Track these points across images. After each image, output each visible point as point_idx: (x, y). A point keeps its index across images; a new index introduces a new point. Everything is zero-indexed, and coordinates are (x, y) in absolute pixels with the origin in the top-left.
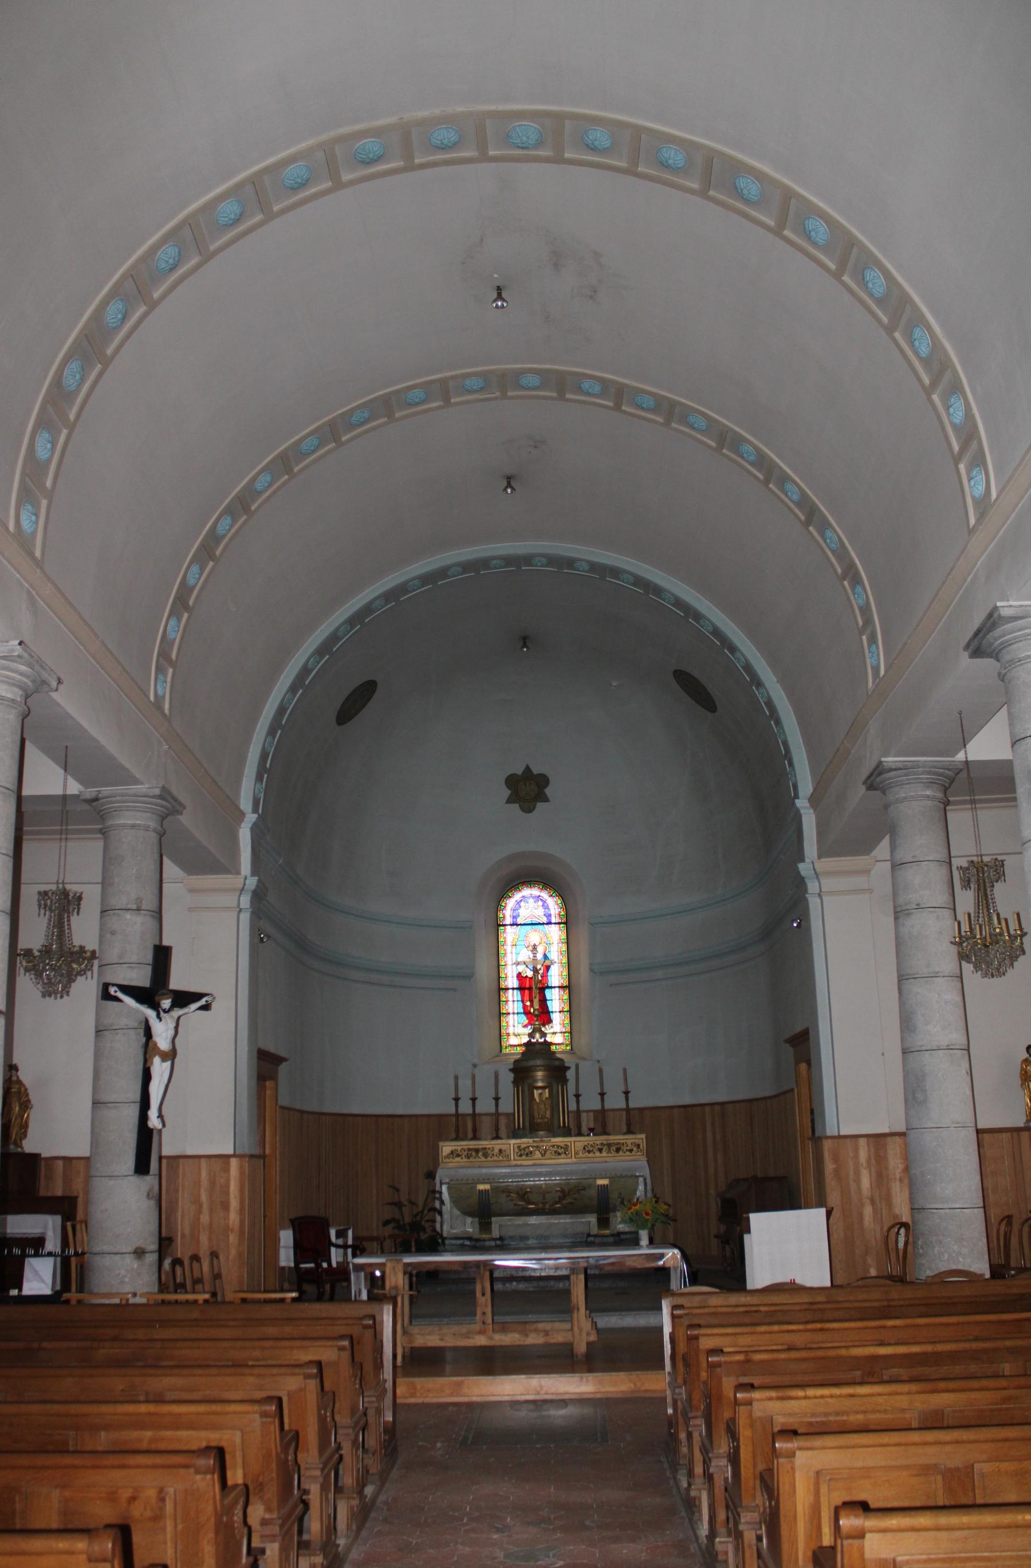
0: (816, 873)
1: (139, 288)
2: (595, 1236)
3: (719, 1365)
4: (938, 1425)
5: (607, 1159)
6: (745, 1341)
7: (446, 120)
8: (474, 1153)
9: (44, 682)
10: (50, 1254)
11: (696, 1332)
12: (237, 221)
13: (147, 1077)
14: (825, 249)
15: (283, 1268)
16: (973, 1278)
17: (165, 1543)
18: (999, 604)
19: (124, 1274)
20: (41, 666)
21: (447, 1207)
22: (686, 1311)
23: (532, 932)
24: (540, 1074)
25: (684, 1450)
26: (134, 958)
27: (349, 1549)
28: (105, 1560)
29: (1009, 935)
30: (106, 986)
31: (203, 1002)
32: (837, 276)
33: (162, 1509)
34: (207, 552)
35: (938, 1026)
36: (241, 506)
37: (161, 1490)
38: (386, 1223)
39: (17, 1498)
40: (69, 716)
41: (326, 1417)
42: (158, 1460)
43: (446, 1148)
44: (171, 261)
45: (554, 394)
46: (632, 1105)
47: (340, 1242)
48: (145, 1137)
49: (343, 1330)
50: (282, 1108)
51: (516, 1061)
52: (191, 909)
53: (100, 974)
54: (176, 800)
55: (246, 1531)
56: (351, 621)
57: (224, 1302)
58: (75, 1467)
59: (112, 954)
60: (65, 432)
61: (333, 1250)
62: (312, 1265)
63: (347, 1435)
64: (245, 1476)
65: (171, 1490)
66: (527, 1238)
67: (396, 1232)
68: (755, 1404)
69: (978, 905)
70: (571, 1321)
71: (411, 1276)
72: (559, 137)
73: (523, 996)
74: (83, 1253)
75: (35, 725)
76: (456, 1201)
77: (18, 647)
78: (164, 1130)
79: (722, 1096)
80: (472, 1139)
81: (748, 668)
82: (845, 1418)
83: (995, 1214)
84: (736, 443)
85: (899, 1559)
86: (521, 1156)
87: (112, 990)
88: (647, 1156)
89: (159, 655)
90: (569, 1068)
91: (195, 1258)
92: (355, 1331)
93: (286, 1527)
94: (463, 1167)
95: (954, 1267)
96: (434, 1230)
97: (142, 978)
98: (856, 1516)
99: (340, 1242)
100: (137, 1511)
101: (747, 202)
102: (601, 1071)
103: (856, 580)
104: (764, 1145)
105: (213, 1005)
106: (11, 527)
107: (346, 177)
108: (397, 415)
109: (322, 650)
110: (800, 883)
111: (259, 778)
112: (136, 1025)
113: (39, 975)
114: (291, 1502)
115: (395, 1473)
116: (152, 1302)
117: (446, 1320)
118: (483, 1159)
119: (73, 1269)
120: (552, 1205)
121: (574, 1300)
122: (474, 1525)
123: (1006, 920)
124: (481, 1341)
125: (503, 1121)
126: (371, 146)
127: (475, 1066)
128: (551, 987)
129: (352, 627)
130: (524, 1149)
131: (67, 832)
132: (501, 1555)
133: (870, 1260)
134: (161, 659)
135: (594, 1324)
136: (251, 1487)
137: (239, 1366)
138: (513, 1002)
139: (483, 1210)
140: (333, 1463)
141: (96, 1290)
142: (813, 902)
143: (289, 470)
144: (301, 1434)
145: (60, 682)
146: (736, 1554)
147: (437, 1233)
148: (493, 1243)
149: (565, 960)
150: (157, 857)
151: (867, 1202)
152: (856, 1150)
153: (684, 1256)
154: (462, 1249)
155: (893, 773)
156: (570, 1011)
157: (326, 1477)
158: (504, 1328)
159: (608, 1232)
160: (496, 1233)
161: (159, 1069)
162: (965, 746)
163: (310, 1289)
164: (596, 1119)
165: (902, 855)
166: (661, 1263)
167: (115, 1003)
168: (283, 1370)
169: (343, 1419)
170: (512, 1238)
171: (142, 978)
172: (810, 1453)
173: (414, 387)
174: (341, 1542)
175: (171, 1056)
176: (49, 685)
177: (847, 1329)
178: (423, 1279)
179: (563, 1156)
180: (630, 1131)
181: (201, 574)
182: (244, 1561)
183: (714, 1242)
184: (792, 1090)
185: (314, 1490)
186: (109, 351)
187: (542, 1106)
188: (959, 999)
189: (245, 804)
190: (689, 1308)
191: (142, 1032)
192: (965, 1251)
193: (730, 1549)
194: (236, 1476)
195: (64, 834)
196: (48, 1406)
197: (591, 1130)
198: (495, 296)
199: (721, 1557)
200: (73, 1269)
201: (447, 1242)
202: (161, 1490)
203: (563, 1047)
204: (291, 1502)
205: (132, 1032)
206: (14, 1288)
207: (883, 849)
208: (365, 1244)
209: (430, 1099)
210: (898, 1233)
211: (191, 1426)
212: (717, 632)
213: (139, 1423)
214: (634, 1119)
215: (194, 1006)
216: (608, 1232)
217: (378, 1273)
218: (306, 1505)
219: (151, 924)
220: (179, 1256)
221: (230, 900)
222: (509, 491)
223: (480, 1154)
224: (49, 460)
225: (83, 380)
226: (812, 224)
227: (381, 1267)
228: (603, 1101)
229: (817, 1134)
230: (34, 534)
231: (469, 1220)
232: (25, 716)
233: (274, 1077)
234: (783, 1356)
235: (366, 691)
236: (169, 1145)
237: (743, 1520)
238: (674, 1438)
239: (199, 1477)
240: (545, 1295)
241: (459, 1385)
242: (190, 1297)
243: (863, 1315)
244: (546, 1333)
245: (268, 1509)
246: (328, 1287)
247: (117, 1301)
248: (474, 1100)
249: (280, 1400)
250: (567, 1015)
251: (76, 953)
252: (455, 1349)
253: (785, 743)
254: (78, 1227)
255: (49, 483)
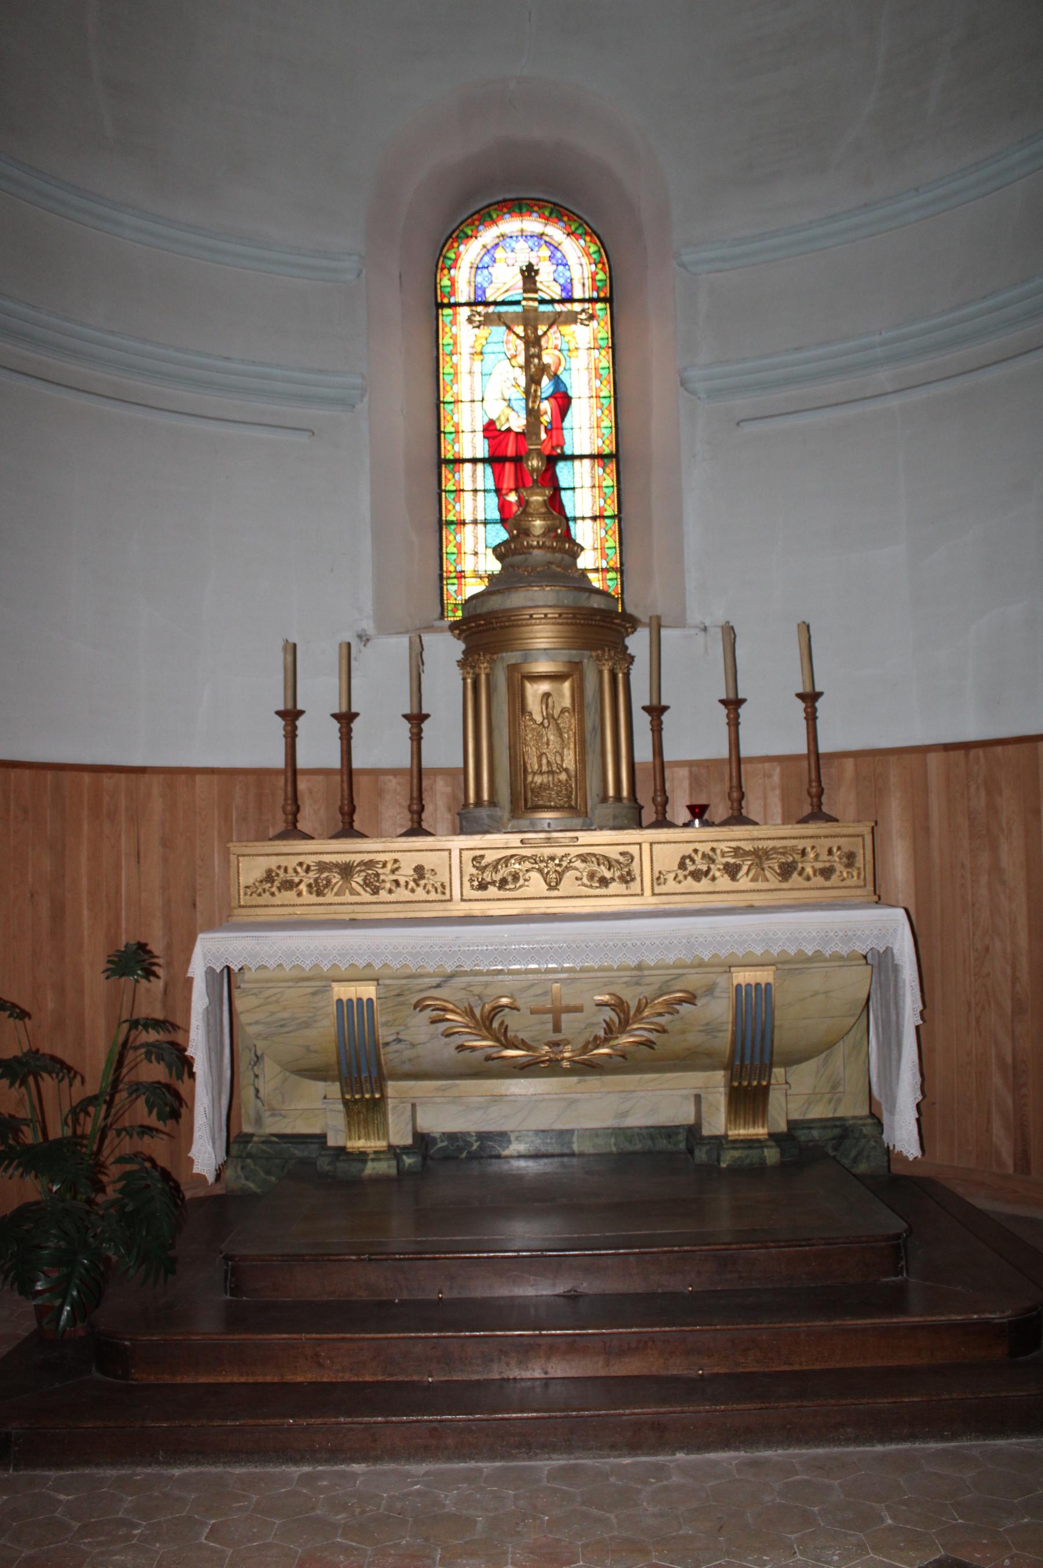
4: (462, 777)
8: (336, 879)
73: (498, 478)
80: (651, 826)
86: (483, 886)
120: (585, 1049)
128: (573, 458)
130: (495, 866)
149: (606, 391)
156: (618, 517)
179: (615, 887)
197: (698, 811)
216: (760, 1131)
248: (346, 719)
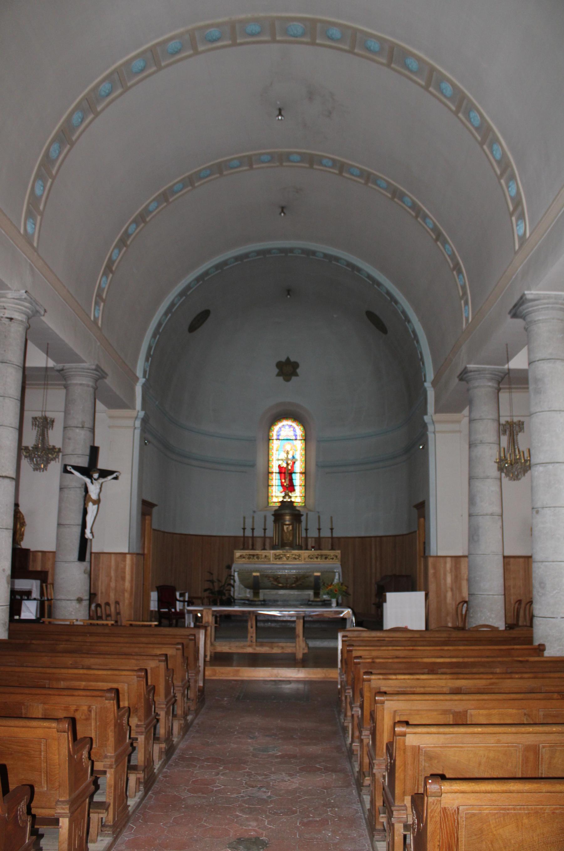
0: (433, 421)
1: (90, 105)
2: (312, 601)
3: (359, 663)
5: (321, 563)
6: (374, 654)
7: (256, 20)
9: (37, 312)
10: (35, 599)
11: (351, 648)
12: (142, 70)
13: (85, 512)
14: (451, 99)
15: (152, 611)
16: (494, 629)
17: (91, 730)
18: (526, 292)
19: (71, 610)
20: (37, 304)
21: (237, 583)
22: (349, 639)
23: (287, 444)
24: (288, 518)
25: (344, 705)
26: (80, 452)
27: (178, 743)
28: (64, 732)
29: (525, 460)
30: (65, 466)
31: (114, 475)
32: (456, 113)
33: (90, 715)
34: (123, 242)
35: (488, 504)
36: (142, 218)
37: (90, 707)
38: (205, 590)
39: (23, 707)
40: (49, 328)
41: (169, 680)
42: (88, 693)
43: (238, 553)
44: (107, 91)
45: (307, 165)
46: (334, 535)
47: (182, 599)
48: (84, 543)
49: (179, 641)
50: (154, 530)
51: (276, 511)
52: (110, 427)
53: (63, 459)
54: (102, 370)
55: (128, 728)
56: (198, 279)
57: (121, 626)
58: (50, 695)
59: (69, 450)
60: (50, 180)
61: (178, 603)
62: (166, 610)
63: (179, 690)
64: (129, 704)
65: (94, 707)
66: (277, 601)
67: (211, 595)
68: (372, 681)
69: (509, 443)
70: (295, 642)
71: (216, 617)
72: (313, 32)
74: (51, 599)
75: (33, 333)
76: (242, 580)
77: (25, 294)
78: (93, 540)
79: (381, 533)
81: (404, 312)
82: (415, 689)
83: (513, 599)
84: (402, 196)
85: (421, 746)
86: (276, 559)
87: (69, 468)
88: (341, 561)
89: (97, 296)
90: (302, 515)
91: (108, 604)
92: (185, 641)
93: (148, 729)
94: (246, 564)
95: (487, 623)
96: (230, 595)
97: (84, 462)
98: (403, 727)
99: (182, 599)
100: (78, 716)
101: (411, 71)
102: (319, 517)
103: (460, 272)
104: (399, 559)
105: (120, 478)
106: (22, 231)
107: (201, 48)
108: (225, 173)
109: (182, 294)
110: (425, 426)
111: (147, 360)
112: (80, 486)
113: (32, 460)
114: (150, 718)
115: (203, 711)
116: (85, 624)
117: (233, 640)
118: (256, 560)
119: (46, 607)
121: (297, 632)
122: (240, 735)
123: (523, 452)
124: (249, 650)
125: (268, 541)
126: (215, 32)
127: (254, 512)
129: (198, 282)
130: (278, 555)
131: (47, 384)
132: (251, 749)
133: (449, 619)
134: (98, 298)
135: (307, 645)
136: (132, 710)
137: (127, 655)
138: (275, 480)
139: (255, 585)
140: (172, 702)
141: (57, 618)
142: (431, 436)
143: (167, 200)
144: (156, 688)
145: (45, 311)
146: (360, 750)
147: (231, 597)
148: (260, 603)
149: (303, 459)
150: (93, 401)
151: (449, 590)
152: (445, 563)
153: (354, 613)
154: (244, 605)
155: (472, 373)
157: (168, 708)
158: (262, 645)
159: (318, 599)
160: (261, 597)
161: (92, 508)
162: (508, 361)
163: (165, 622)
164: (316, 542)
165: (476, 415)
166: (342, 615)
167: (70, 475)
168: (148, 657)
169: (178, 683)
170: (270, 601)
171: (84, 462)
172: (392, 702)
173: (235, 159)
174: (175, 740)
175: (97, 502)
176: (40, 313)
177: (425, 650)
178: (223, 620)
180: (332, 549)
181: (119, 254)
182: (127, 741)
183: (373, 607)
184: (415, 532)
185: (162, 714)
186: (74, 138)
187: (288, 534)
188: (498, 490)
189: (139, 373)
190: (350, 637)
191: (83, 490)
192: (493, 616)
193: (359, 748)
194: (124, 703)
195: (46, 386)
196: (36, 669)
197: (313, 547)
198: (278, 112)
199: (355, 753)
200: (46, 607)
201: (236, 601)
202: (90, 707)
203: (301, 504)
204: (150, 718)
205: (78, 490)
206: (17, 615)
207: (466, 411)
208: (194, 600)
209: (232, 529)
210: (463, 606)
211: (103, 681)
212: (388, 293)
213: (80, 678)
214: (335, 543)
215: (110, 477)
216: (318, 599)
217: (199, 615)
218: (158, 720)
219: (89, 434)
220: (99, 602)
221: (130, 423)
222: (282, 214)
223: (255, 557)
224: (41, 196)
225: (60, 153)
226: (444, 85)
227: (201, 612)
228: (319, 532)
229: (426, 554)
230: (33, 234)
231: (248, 590)
232: (27, 329)
233: (150, 514)
234: (390, 660)
235: (204, 315)
236: (95, 547)
237: (363, 734)
238: (340, 700)
239: (107, 701)
240: (284, 629)
241: (238, 671)
242: (105, 622)
243: (436, 644)
244: (283, 648)
245: (140, 720)
246: (174, 621)
247: (68, 623)
248: (253, 529)
249: (146, 670)
250: (304, 487)
251: (51, 449)
252: (238, 654)
253: (421, 353)
254: (49, 586)
255: (41, 207)
